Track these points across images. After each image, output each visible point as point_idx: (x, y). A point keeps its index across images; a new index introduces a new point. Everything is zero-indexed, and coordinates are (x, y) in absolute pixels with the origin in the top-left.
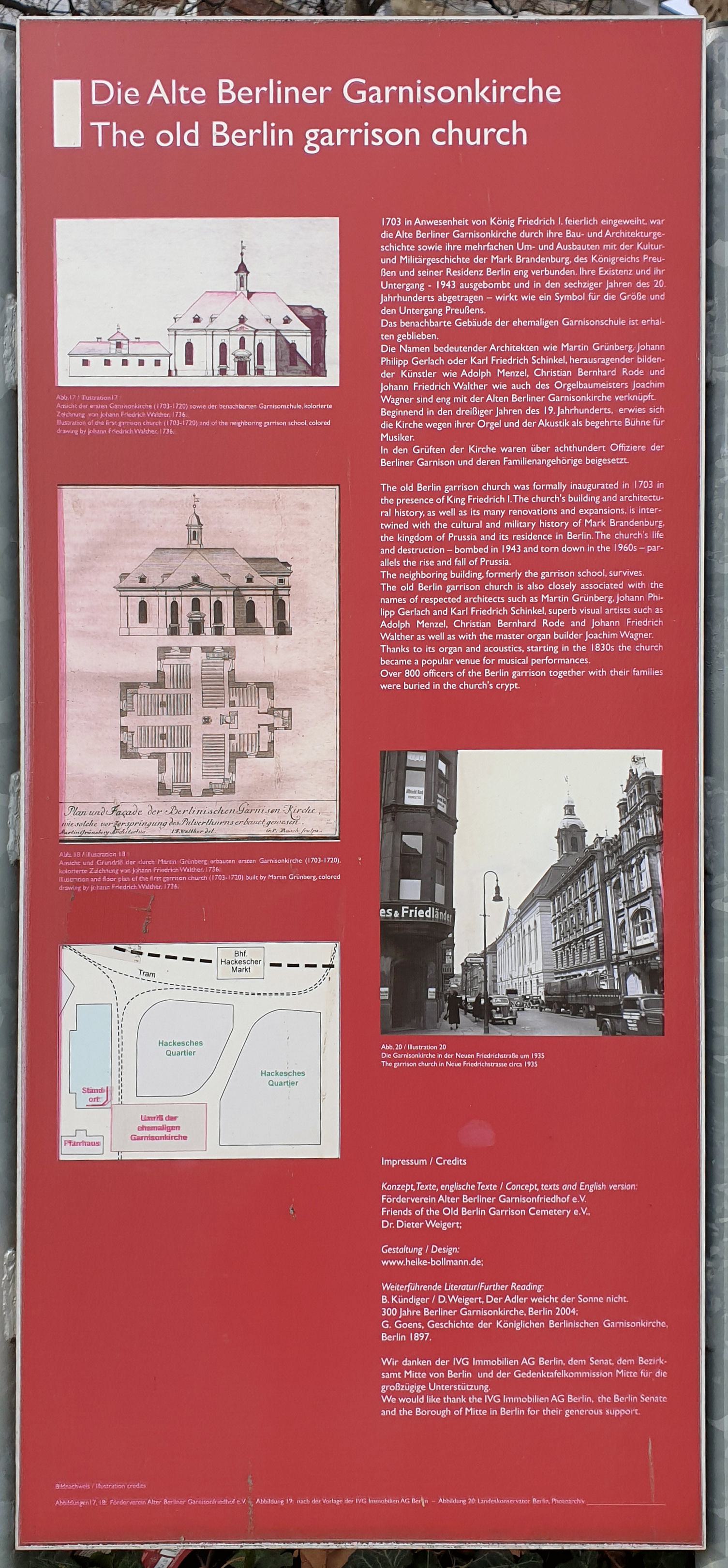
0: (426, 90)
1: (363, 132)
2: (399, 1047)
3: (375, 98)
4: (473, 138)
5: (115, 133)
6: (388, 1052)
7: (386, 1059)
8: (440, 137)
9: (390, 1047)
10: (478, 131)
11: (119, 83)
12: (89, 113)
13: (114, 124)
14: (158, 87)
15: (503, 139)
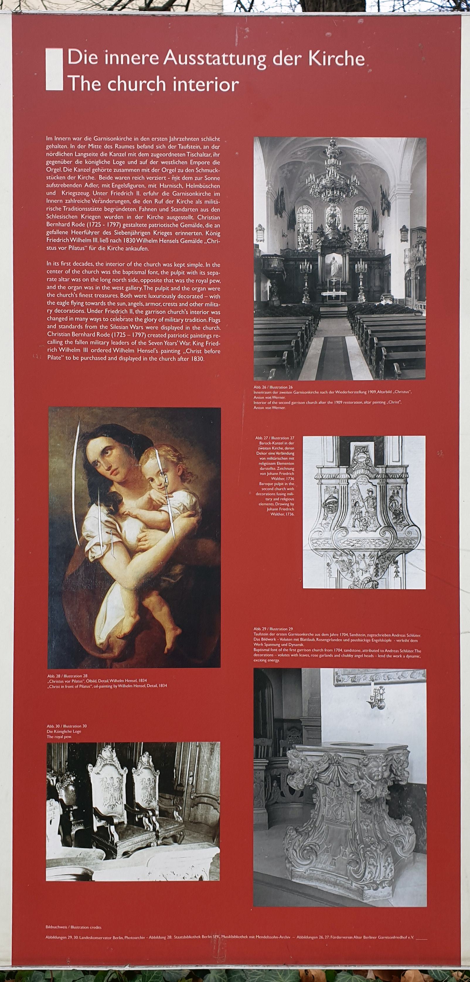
0: (190, 57)
1: (214, 83)
2: (58, 726)
3: (216, 62)
4: (133, 87)
5: (83, 82)
6: (51, 729)
7: (49, 734)
8: (113, 86)
9: (52, 727)
10: (136, 82)
11: (85, 51)
12: (68, 69)
13: (83, 77)
14: (170, 54)
15: (112, 87)
